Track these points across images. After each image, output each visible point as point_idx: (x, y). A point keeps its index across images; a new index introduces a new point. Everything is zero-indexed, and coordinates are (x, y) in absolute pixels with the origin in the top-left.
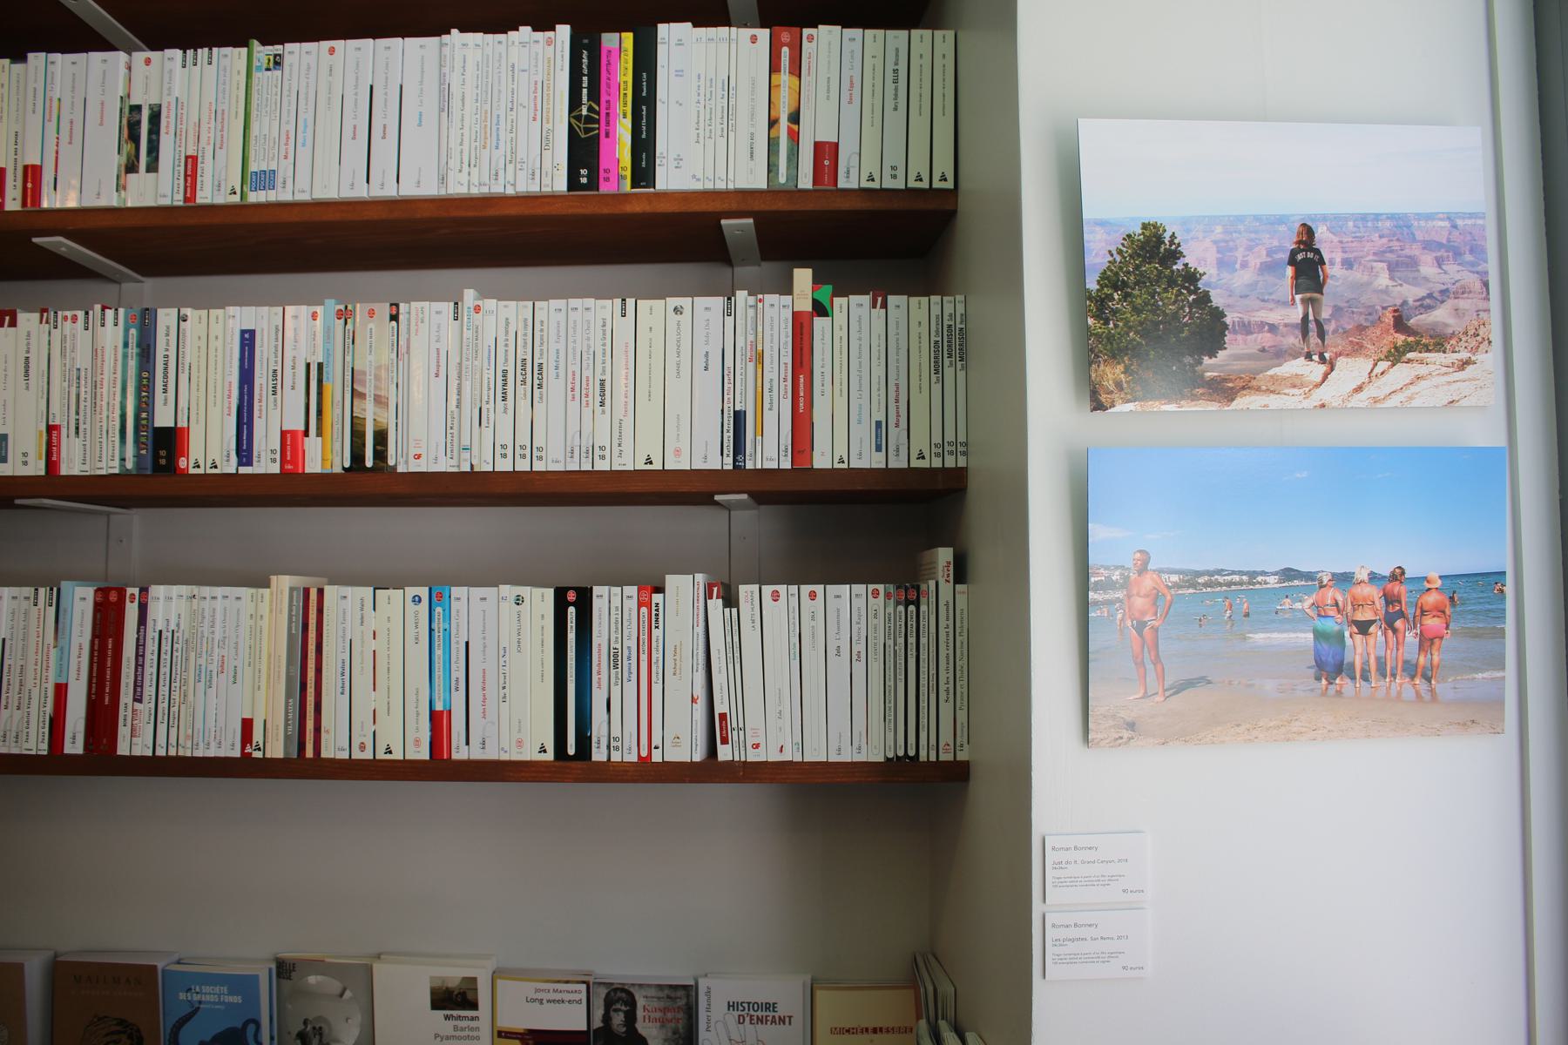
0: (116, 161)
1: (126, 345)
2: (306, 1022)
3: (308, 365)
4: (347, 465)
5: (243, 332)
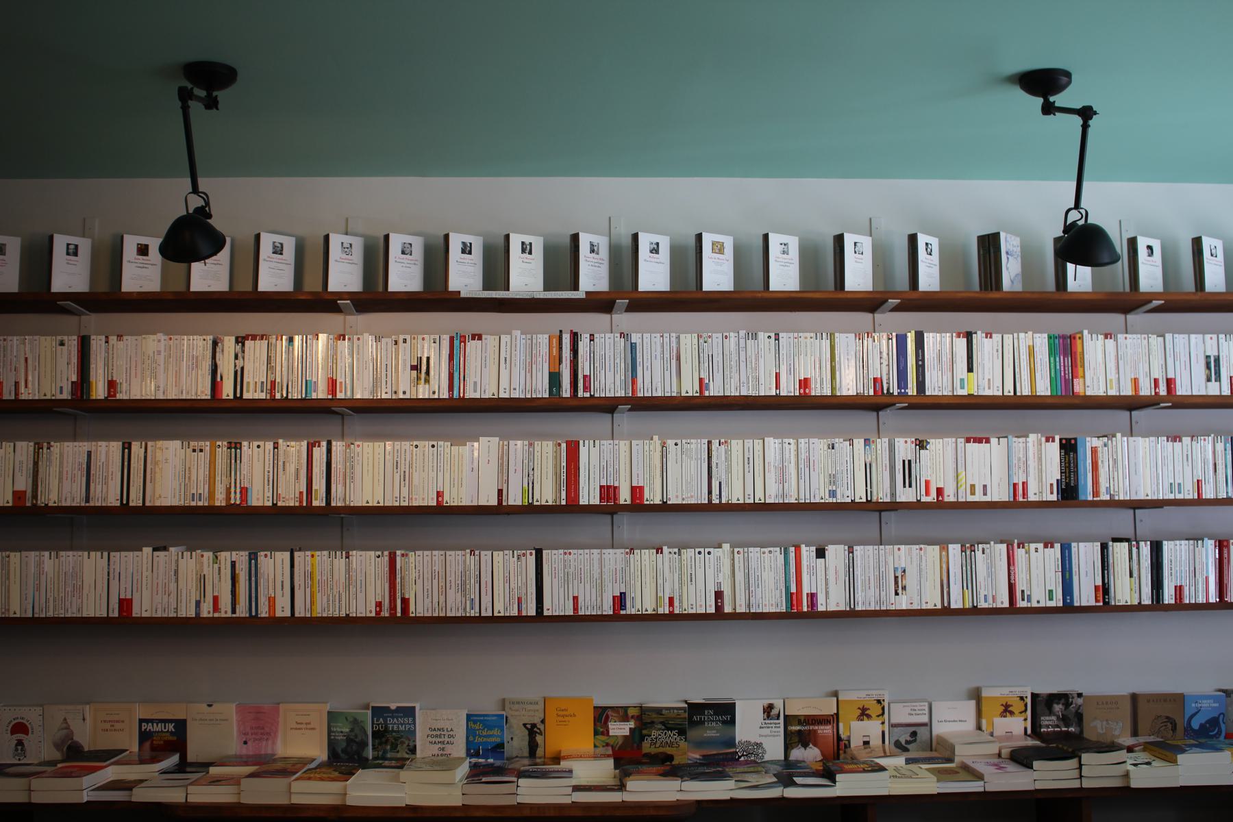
0: (1204, 378)
1: (1225, 450)
3: (904, 461)
5: (88, 452)
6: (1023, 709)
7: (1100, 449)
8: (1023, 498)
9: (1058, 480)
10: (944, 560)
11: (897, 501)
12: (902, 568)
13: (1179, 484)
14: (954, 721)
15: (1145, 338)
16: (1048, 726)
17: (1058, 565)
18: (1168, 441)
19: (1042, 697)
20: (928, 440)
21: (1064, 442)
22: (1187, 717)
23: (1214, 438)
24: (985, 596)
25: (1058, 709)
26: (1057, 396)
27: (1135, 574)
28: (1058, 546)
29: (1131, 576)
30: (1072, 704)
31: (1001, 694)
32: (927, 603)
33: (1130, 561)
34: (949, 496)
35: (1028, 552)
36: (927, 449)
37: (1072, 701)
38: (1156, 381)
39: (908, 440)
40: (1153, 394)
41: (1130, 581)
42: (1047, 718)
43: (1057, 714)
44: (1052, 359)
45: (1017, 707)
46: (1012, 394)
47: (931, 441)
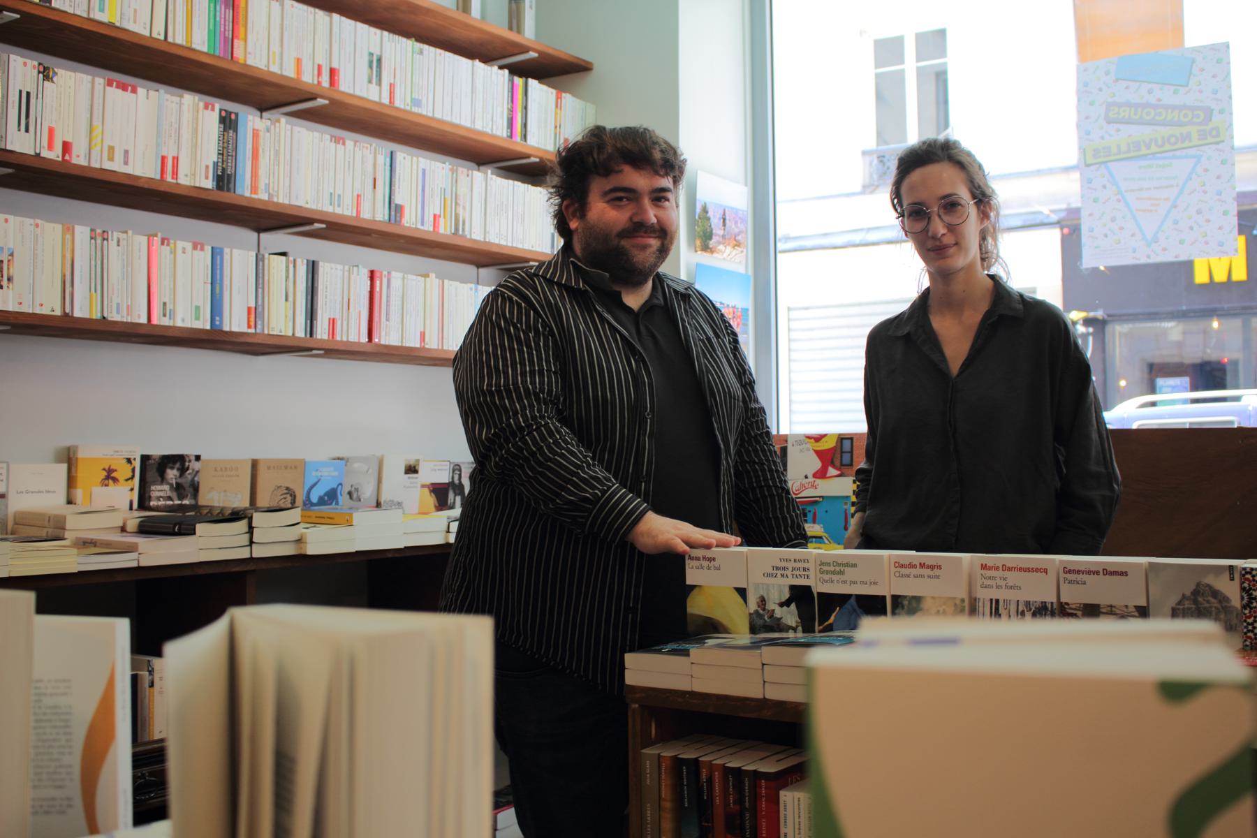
1: (385, 165)
2: (352, 486)
3: (20, 91)
4: (453, 232)
6: (130, 475)
7: (261, 134)
8: (173, 178)
9: (214, 162)
10: (69, 246)
11: (8, 148)
12: (9, 249)
13: (339, 196)
14: (40, 492)
15: (311, 13)
16: (158, 499)
17: (207, 274)
18: (331, 141)
19: (155, 460)
20: (56, 70)
21: (224, 114)
22: (307, 488)
23: (375, 150)
24: (118, 304)
25: (172, 476)
26: (213, 56)
27: (291, 298)
28: (208, 249)
29: (287, 300)
30: (188, 469)
31: (104, 455)
32: (42, 305)
33: (286, 280)
34: (78, 156)
35: (174, 252)
36: (53, 82)
37: (189, 466)
38: (320, 67)
39: (29, 62)
40: (316, 82)
41: (286, 305)
42: (159, 487)
43: (171, 482)
44: (212, 5)
45: (123, 472)
46: (162, 37)
47: (60, 72)
